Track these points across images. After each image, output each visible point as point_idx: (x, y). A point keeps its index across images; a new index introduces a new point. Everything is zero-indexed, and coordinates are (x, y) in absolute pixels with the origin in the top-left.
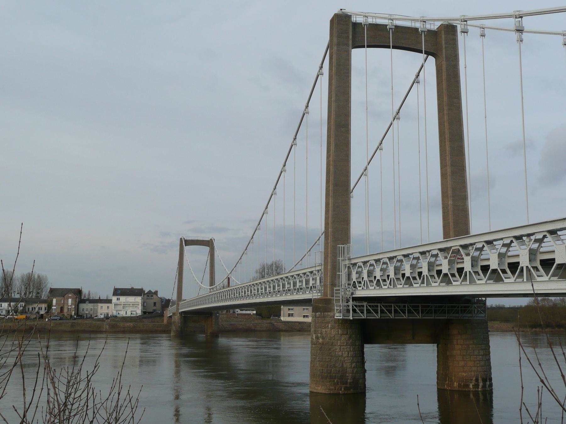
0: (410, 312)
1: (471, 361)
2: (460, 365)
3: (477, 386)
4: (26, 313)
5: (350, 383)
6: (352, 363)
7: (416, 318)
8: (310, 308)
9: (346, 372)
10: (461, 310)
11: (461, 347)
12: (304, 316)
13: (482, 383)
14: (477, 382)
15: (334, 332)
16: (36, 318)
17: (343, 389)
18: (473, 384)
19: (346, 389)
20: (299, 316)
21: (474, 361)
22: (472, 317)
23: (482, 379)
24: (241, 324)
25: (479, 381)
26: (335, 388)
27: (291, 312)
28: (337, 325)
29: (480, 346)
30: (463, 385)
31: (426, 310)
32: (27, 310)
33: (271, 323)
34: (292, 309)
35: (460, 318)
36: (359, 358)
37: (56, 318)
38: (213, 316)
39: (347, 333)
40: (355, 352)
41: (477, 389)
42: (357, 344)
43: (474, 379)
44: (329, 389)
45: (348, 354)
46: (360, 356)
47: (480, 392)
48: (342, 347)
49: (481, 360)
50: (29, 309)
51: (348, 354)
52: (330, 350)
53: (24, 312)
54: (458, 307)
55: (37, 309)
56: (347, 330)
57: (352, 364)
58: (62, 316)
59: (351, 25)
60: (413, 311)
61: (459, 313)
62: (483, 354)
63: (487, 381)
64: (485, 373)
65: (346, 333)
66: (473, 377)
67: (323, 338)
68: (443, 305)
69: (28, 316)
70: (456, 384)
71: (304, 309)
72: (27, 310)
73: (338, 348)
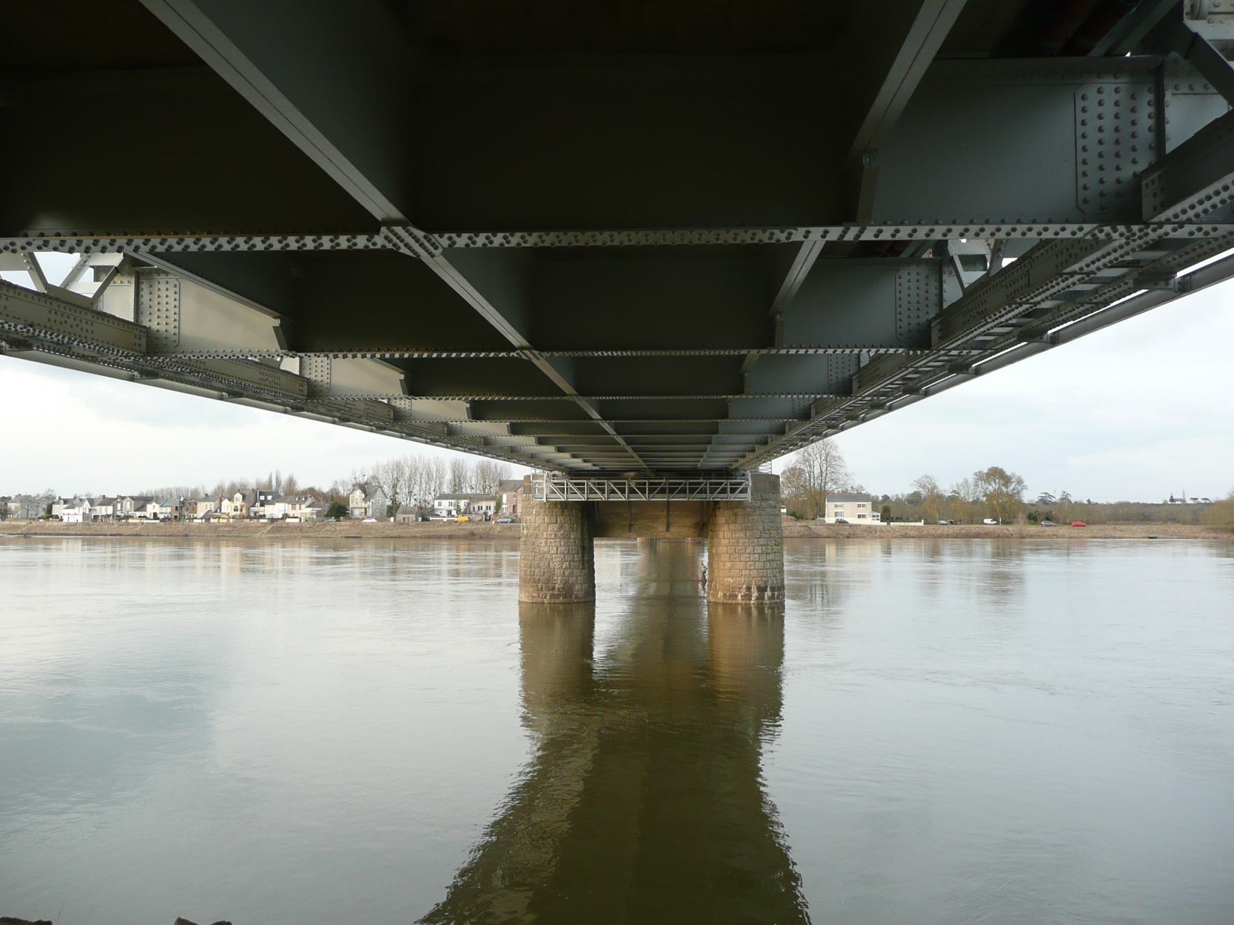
0: (591, 491)
1: (741, 561)
2: (726, 568)
3: (748, 596)
4: (470, 513)
6: (562, 562)
7: (641, 499)
8: (869, 505)
9: (554, 574)
11: (728, 542)
12: (836, 513)
15: (539, 520)
16: (480, 520)
17: (548, 597)
19: (552, 596)
22: (727, 498)
25: (752, 590)
26: (539, 595)
27: (838, 510)
28: (542, 511)
29: (756, 540)
32: (472, 509)
33: (807, 526)
34: (841, 506)
35: (708, 500)
36: (576, 555)
37: (506, 520)
39: (557, 521)
41: (748, 602)
43: (744, 586)
44: (532, 597)
45: (557, 549)
46: (578, 553)
47: (752, 606)
49: (757, 559)
50: (474, 508)
51: (557, 549)
52: (533, 544)
53: (468, 512)
54: (686, 484)
55: (484, 508)
56: (557, 518)
57: (562, 564)
58: (515, 518)
59: (1133, 56)
60: (637, 490)
61: (706, 493)
62: (760, 551)
63: (766, 590)
66: (743, 584)
67: (528, 529)
69: (471, 517)
70: (720, 594)
71: (859, 506)
72: (472, 509)
73: (543, 541)
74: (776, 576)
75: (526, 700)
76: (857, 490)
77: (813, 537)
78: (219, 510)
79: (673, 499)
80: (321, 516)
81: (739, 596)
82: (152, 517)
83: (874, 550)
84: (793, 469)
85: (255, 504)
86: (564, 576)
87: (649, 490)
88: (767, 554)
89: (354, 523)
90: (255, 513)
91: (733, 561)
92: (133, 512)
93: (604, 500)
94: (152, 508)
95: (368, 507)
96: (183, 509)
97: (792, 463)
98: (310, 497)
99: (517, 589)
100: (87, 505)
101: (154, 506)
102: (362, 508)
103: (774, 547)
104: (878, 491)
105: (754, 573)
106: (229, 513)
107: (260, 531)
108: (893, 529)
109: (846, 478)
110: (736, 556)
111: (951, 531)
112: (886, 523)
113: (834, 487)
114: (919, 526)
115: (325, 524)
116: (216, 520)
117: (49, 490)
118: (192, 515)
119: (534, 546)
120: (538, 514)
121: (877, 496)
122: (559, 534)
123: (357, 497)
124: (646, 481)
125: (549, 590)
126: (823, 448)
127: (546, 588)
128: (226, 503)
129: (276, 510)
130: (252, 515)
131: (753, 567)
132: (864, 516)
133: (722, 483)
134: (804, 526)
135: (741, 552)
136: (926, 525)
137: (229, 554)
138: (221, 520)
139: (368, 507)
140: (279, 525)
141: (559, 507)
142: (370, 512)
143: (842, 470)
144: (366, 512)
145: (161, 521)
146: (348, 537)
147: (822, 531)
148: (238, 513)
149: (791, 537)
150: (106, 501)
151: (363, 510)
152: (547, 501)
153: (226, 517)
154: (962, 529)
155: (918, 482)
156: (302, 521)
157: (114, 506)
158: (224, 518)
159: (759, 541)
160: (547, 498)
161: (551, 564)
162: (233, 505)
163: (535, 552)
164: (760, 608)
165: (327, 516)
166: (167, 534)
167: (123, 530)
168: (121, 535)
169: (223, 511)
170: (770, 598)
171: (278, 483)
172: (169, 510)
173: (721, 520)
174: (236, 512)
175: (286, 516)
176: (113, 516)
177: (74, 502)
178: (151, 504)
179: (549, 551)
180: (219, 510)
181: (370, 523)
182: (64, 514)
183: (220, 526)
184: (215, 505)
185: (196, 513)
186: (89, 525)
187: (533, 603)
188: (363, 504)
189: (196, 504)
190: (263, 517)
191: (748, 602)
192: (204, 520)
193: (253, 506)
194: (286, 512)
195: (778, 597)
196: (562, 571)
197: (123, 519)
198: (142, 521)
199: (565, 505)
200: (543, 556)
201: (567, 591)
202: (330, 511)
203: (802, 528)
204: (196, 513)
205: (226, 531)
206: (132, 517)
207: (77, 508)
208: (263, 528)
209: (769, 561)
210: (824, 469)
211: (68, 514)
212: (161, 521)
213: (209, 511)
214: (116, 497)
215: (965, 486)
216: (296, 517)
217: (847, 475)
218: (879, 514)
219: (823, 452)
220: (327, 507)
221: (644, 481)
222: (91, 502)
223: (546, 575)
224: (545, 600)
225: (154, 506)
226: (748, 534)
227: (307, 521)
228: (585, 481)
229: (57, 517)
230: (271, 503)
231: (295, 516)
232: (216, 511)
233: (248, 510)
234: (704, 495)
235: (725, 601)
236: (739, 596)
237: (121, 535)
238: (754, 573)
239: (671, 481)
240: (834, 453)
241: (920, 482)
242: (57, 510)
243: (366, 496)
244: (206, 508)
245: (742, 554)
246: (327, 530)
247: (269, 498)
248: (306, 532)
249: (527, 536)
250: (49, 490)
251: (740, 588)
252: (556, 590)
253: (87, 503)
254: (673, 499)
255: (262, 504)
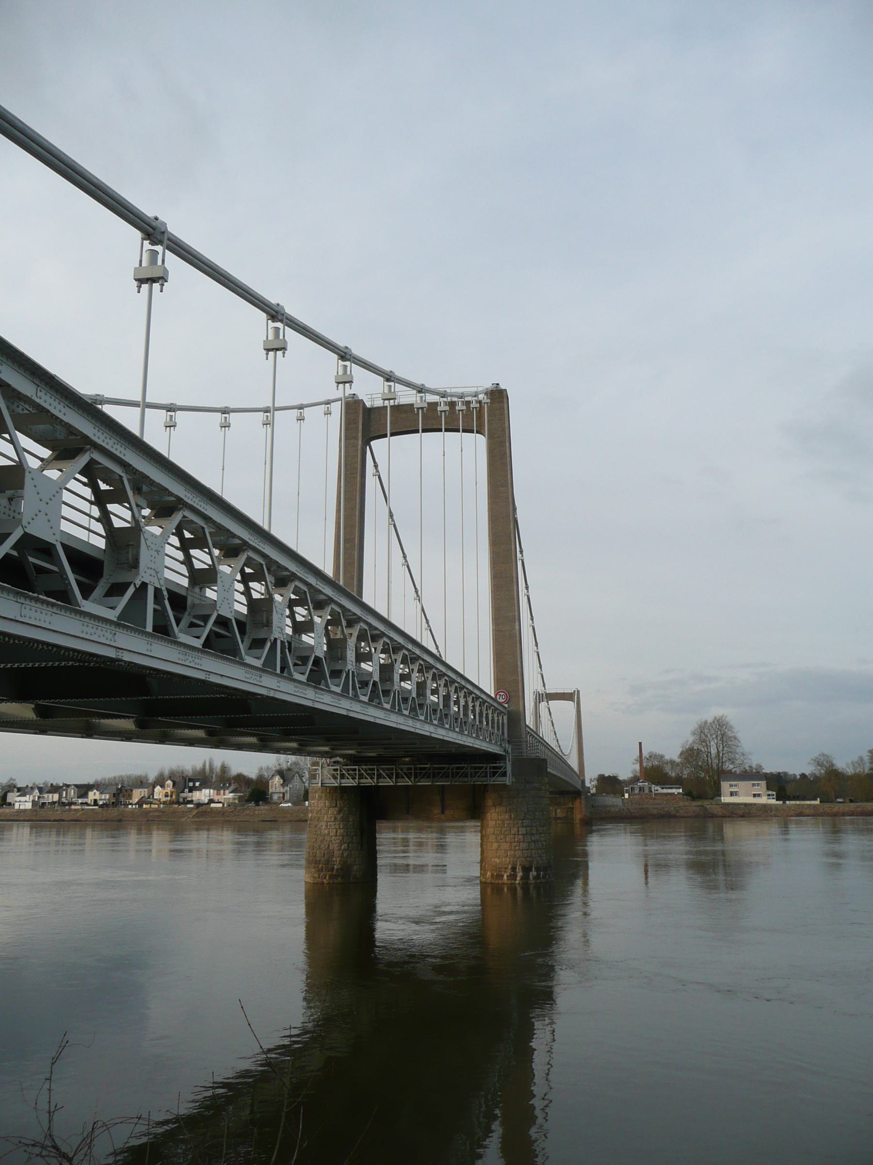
1: (506, 842)
3: (513, 876)
5: (337, 869)
7: (408, 784)
8: (763, 783)
10: (452, 773)
13: (522, 872)
14: (513, 871)
15: (321, 804)
17: (327, 878)
18: (508, 874)
19: (331, 877)
20: (747, 795)
21: (511, 843)
23: (522, 868)
24: (657, 808)
25: (517, 870)
26: (319, 875)
27: (733, 789)
28: (324, 795)
29: (520, 821)
30: (496, 875)
31: (475, 773)
33: (702, 806)
34: (736, 786)
35: (469, 783)
36: (354, 838)
38: (583, 797)
40: (346, 830)
41: (513, 882)
42: (351, 820)
43: (510, 867)
45: (337, 832)
47: (517, 885)
48: (329, 824)
51: (337, 832)
52: (316, 827)
56: (336, 802)
57: (341, 845)
61: (486, 776)
64: (528, 859)
65: (334, 805)
66: (508, 865)
68: (483, 765)
70: (489, 874)
71: (754, 785)
73: (324, 824)
74: (541, 856)
75: (308, 985)
76: (756, 769)
77: (708, 816)
78: (151, 796)
79: (437, 783)
80: (242, 801)
81: (505, 876)
82: (93, 803)
83: (772, 829)
84: (691, 749)
85: (184, 790)
86: (343, 857)
87: (377, 775)
88: (532, 834)
89: (271, 808)
90: (184, 799)
91: (499, 842)
92: (76, 799)
93: (374, 784)
94: (93, 795)
95: (286, 792)
96: (120, 796)
97: (689, 743)
98: (234, 783)
99: (304, 871)
100: (36, 792)
101: (95, 793)
102: (280, 793)
103: (539, 828)
104: (771, 767)
105: (518, 853)
106: (160, 799)
107: (186, 816)
108: (789, 807)
109: (742, 758)
110: (502, 836)
111: (847, 809)
112: (781, 802)
113: (731, 766)
114: (815, 805)
115: (246, 809)
116: (148, 806)
117: (11, 779)
118: (127, 801)
119: (316, 829)
120: (320, 798)
121: (794, 775)
122: (339, 817)
123: (276, 782)
124: (412, 766)
125: (329, 871)
126: (719, 729)
127: (325, 870)
128: (158, 789)
129: (203, 795)
130: (181, 800)
131: (517, 848)
132: (759, 795)
133: (444, 768)
134: (699, 806)
135: (506, 833)
136: (822, 804)
137: (160, 840)
138: (153, 806)
139: (286, 792)
140: (204, 810)
141: (339, 791)
142: (287, 797)
143: (738, 750)
144: (284, 797)
145: (99, 807)
146: (264, 821)
147: (717, 810)
148: (169, 798)
149: (686, 817)
150: (54, 789)
151: (281, 795)
152: (322, 786)
153: (157, 802)
154: (858, 807)
155: (815, 761)
156: (225, 806)
157: (59, 794)
158: (155, 804)
159: (523, 823)
160: (322, 784)
161: (331, 846)
162: (164, 792)
163: (317, 835)
164: (525, 886)
165: (248, 801)
166: (103, 819)
167: (65, 816)
168: (63, 820)
169: (155, 797)
170: (535, 878)
171: (211, 769)
172: (107, 796)
173: (489, 802)
174: (167, 798)
175: (211, 801)
176: (59, 803)
177: (26, 791)
178: (92, 791)
179: (329, 833)
180: (151, 796)
181: (286, 807)
182: (16, 802)
183: (151, 812)
184: (148, 791)
185: (131, 799)
186: (36, 811)
187: (314, 883)
188: (282, 789)
189: (132, 791)
190: (191, 802)
191: (513, 882)
192: (137, 806)
193: (183, 792)
194: (211, 798)
195: (544, 877)
196: (341, 852)
197: (67, 805)
198: (83, 807)
199: (343, 790)
200: (324, 838)
201: (345, 870)
202: (250, 796)
203: (698, 808)
204: (131, 799)
205: (156, 816)
206: (75, 804)
207: (28, 796)
208: (189, 813)
209: (534, 842)
210: (720, 749)
211: (20, 801)
212: (99, 807)
213: (143, 797)
214: (61, 785)
215: (861, 763)
216: (220, 802)
217: (743, 755)
218: (775, 793)
219: (719, 732)
220: (248, 792)
221: (392, 767)
222: (41, 790)
223: (326, 856)
224: (325, 880)
225: (95, 793)
226: (512, 816)
227: (229, 805)
228: (357, 767)
229: (10, 804)
230: (199, 789)
231: (220, 801)
232: (149, 798)
233: (178, 796)
234: (465, 779)
235: (493, 881)
236: (505, 876)
237: (63, 820)
238: (518, 853)
239: (435, 766)
240: (730, 734)
241: (817, 760)
242: (12, 797)
243: (284, 781)
244: (141, 795)
245: (508, 834)
246: (247, 814)
247: (197, 784)
248: (228, 817)
249: (311, 820)
250: (11, 779)
251: (506, 868)
252: (335, 871)
253: (37, 791)
254: (437, 783)
255: (191, 791)
